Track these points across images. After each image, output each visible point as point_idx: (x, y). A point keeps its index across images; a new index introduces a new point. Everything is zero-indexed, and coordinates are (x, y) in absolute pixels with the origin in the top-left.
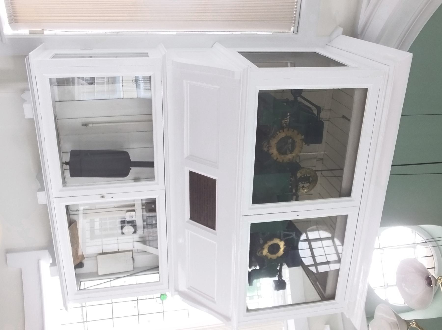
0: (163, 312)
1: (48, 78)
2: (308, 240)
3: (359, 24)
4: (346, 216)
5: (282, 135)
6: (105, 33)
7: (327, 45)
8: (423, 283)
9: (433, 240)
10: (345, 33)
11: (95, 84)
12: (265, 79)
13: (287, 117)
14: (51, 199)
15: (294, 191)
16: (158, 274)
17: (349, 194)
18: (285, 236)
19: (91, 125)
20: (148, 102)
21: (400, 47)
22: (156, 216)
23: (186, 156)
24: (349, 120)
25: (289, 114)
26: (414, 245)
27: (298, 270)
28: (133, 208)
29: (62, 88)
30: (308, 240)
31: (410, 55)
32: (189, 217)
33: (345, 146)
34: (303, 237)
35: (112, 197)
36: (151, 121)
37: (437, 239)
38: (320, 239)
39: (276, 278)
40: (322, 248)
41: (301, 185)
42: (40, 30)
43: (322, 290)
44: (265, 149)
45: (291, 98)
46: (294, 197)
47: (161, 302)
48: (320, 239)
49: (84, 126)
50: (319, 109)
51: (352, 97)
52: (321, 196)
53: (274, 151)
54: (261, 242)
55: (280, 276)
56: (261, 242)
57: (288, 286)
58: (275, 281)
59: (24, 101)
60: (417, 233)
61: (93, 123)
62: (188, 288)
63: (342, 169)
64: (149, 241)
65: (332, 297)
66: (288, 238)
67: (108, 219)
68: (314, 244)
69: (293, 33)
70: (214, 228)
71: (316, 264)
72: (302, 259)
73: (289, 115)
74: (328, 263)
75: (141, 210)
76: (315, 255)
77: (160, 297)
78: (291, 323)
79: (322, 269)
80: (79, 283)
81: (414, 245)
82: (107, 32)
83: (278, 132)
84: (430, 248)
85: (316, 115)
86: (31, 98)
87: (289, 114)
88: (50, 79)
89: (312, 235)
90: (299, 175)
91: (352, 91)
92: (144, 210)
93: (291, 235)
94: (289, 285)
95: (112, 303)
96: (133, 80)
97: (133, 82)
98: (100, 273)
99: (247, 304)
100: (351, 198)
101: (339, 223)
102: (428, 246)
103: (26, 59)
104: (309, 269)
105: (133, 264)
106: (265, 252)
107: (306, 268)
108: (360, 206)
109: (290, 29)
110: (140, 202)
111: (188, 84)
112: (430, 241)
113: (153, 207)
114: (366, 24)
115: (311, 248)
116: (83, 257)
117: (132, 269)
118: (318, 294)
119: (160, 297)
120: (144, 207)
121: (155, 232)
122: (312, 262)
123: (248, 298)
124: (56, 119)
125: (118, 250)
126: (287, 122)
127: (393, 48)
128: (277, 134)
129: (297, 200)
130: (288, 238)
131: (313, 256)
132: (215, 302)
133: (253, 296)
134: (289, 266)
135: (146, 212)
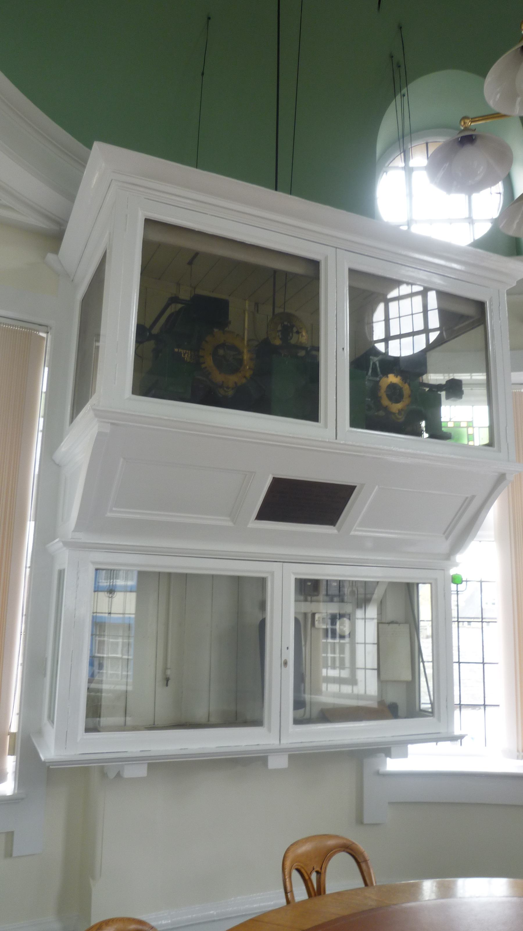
0: (481, 582)
1: (84, 734)
2: (387, 339)
3: (44, 226)
4: (352, 272)
5: (209, 362)
6: (22, 635)
7: (73, 281)
8: (469, 150)
9: (401, 140)
10: (56, 250)
11: (103, 657)
12: (115, 383)
13: (181, 354)
14: (282, 747)
15: (302, 353)
16: (420, 585)
17: (315, 264)
18: (375, 373)
19: (169, 672)
20: (142, 575)
21: (82, 162)
22: (327, 581)
23: (230, 524)
24: (197, 254)
25: (176, 350)
26: (409, 170)
27: (432, 358)
28: (309, 616)
29: (103, 711)
30: (387, 339)
31: (97, 145)
32: (332, 527)
33: (238, 264)
34: (381, 347)
35: (288, 648)
36: (170, 574)
37: (401, 133)
38: (387, 320)
39: (443, 394)
40: (398, 316)
41: (293, 341)
42: (10, 738)
43: (467, 323)
44: (230, 393)
45: (150, 345)
46: (314, 353)
47: (464, 583)
48: (387, 320)
49: (169, 682)
50: (174, 300)
51: (159, 245)
52: (316, 311)
53: (233, 380)
54: (382, 413)
55: (440, 387)
56: (382, 413)
57: (458, 376)
58: (448, 397)
59: (119, 775)
60: (389, 165)
61: (165, 669)
62: (447, 538)
63: (275, 272)
64: (365, 594)
65: (481, 306)
66: (379, 369)
67: (342, 656)
68: (394, 332)
69: (49, 333)
70: (353, 488)
71: (426, 331)
72: (415, 352)
73: (178, 350)
74: (425, 311)
75: (313, 603)
76: (411, 331)
77: (456, 585)
78: (518, 377)
79: (434, 321)
80: (422, 713)
81: (409, 170)
82: (21, 633)
83: (203, 366)
84: (412, 146)
85: (183, 305)
86: (114, 764)
87: (176, 350)
88: (88, 730)
89: (378, 332)
90: (278, 342)
91: (146, 244)
92: (314, 598)
93: (374, 364)
94: (455, 375)
95: (459, 663)
96: (109, 597)
97: (112, 597)
98: (409, 678)
99: (479, 445)
100: (322, 261)
101: (362, 285)
102: (410, 149)
103: (52, 766)
104: (431, 343)
105: (400, 624)
106: (396, 407)
107: (430, 347)
108: (336, 248)
109: (43, 338)
110: (303, 604)
111: (114, 509)
112: (402, 145)
113: (309, 584)
114: (48, 218)
115: (400, 336)
116: (381, 703)
117: (407, 626)
118: (472, 329)
119: (457, 584)
120: (309, 598)
121: (349, 583)
122: (423, 336)
123: (471, 443)
124: (153, 727)
125: (374, 644)
126: (190, 353)
127: (83, 173)
128: (206, 368)
129: (318, 349)
130: (379, 369)
131: (413, 334)
132: (473, 497)
133: (468, 435)
134: (425, 372)
135: (318, 595)
